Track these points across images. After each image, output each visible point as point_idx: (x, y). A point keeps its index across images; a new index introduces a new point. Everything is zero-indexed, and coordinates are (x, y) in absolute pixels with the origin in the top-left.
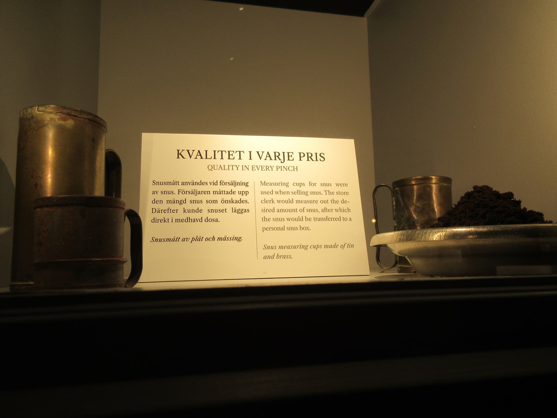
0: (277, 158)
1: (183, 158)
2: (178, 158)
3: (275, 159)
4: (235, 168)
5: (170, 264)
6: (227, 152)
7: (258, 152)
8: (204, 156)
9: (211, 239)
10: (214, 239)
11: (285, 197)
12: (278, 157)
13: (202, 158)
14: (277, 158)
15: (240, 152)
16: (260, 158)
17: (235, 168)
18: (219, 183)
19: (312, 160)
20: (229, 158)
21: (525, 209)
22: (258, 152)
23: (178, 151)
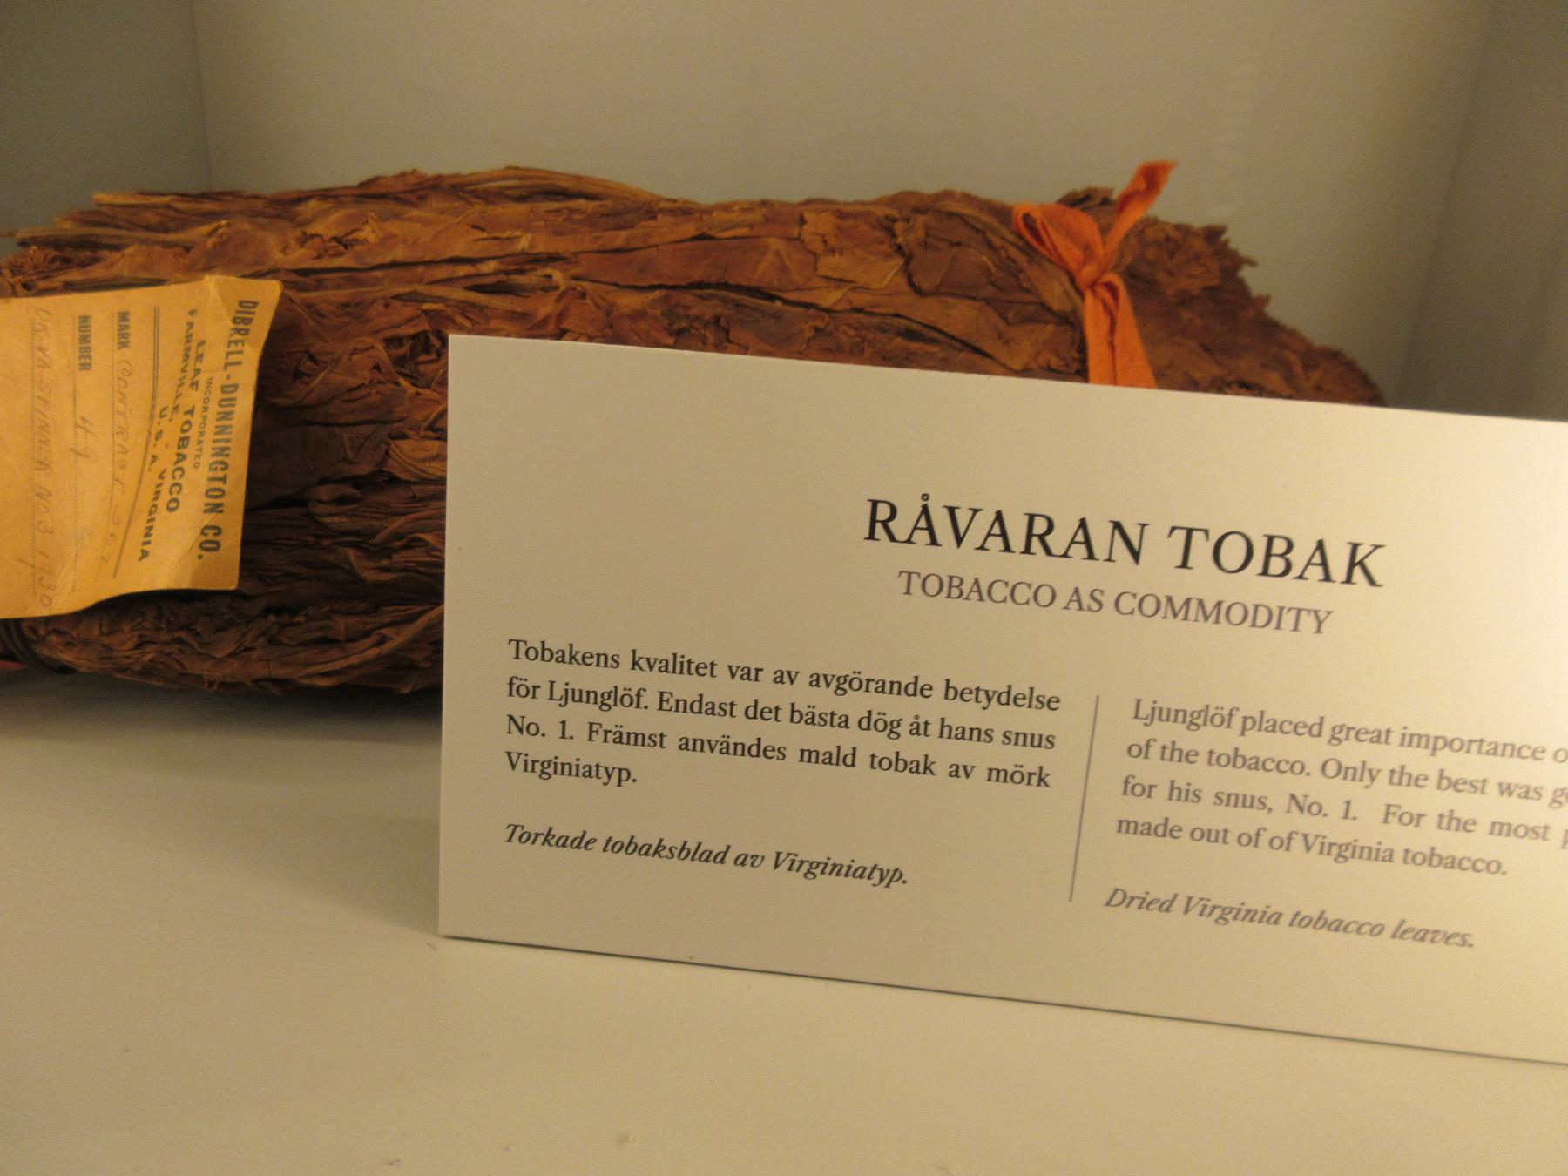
0: (879, 528)
1: (1372, 582)
2: (872, 536)
3: (1027, 551)
4: (1308, 622)
8: (1017, 541)
13: (1007, 549)
14: (879, 528)
15: (1190, 531)
17: (1308, 622)
21: (1227, 241)
23: (1355, 547)
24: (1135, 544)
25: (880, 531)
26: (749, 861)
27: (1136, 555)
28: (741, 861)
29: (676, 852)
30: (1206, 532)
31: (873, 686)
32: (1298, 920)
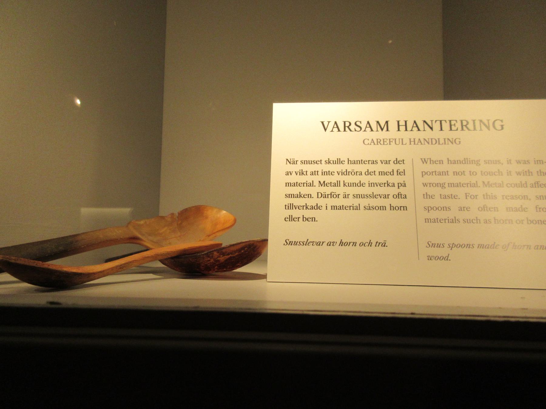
3: (345, 130)
5: (295, 278)
6: (448, 122)
7: (322, 123)
8: (342, 128)
9: (367, 244)
10: (370, 244)
11: (355, 179)
12: (466, 126)
13: (339, 130)
14: (347, 128)
15: (441, 121)
16: (325, 130)
18: (395, 173)
19: (351, 130)
20: (451, 130)
22: (322, 123)
24: (431, 125)
25: (464, 128)
26: (332, 244)
27: (431, 128)
28: (329, 244)
29: (305, 243)
30: (445, 121)
31: (358, 173)
32: (480, 246)
